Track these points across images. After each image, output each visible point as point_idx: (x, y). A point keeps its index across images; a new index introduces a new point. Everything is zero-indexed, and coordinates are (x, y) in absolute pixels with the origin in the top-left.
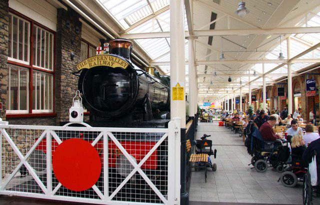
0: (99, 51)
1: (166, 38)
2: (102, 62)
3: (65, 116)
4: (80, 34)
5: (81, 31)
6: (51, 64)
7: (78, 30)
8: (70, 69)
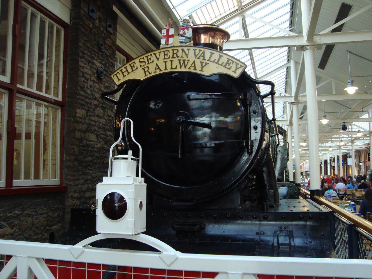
0: (168, 36)
1: (250, 49)
2: (176, 63)
3: (84, 192)
4: (115, 34)
5: (115, 29)
6: (56, 88)
7: (110, 26)
8: (95, 99)
